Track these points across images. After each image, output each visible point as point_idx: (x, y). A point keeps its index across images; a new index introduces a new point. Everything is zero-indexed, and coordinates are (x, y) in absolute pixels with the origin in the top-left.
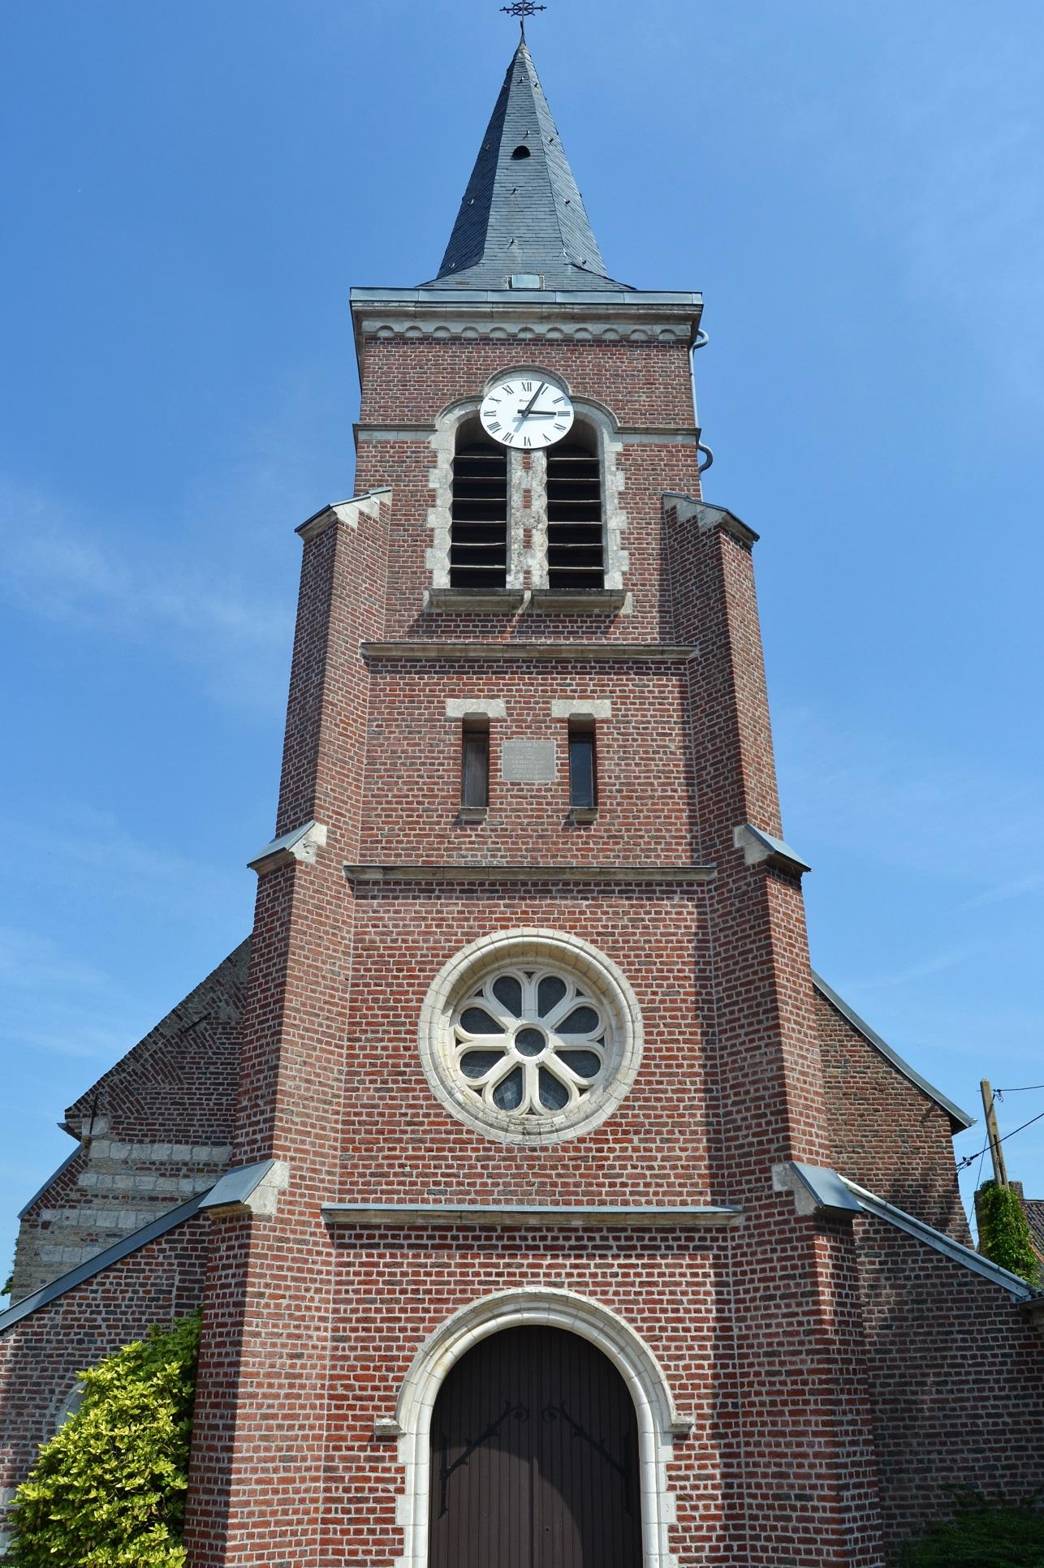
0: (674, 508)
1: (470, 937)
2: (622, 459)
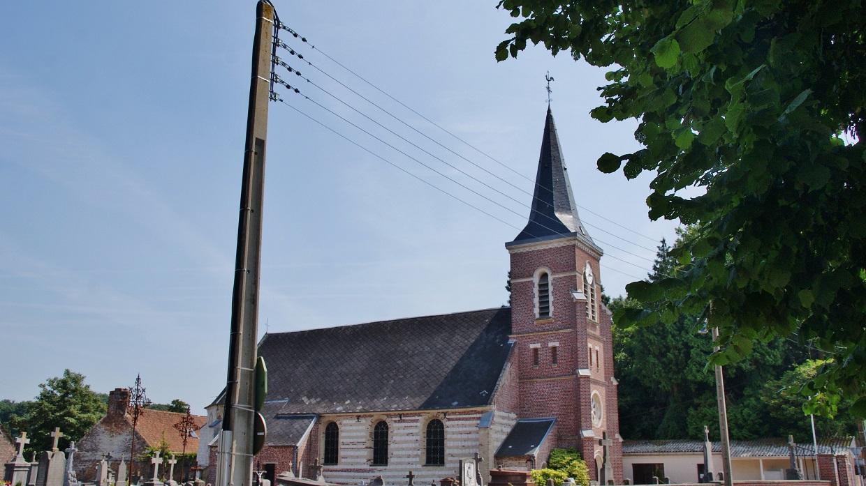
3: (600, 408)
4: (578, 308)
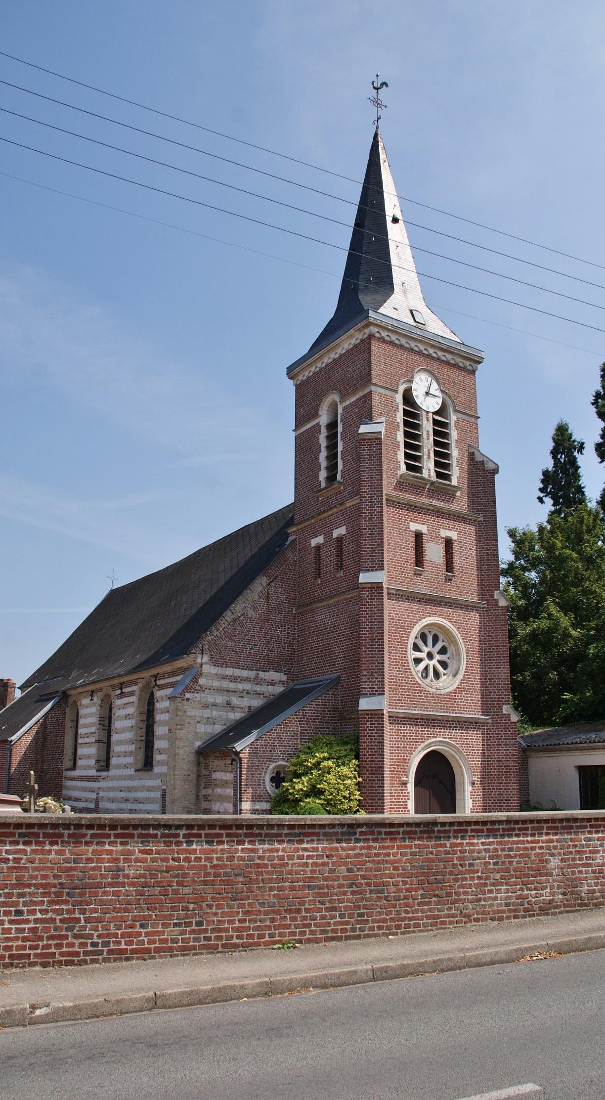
1: (421, 619)
2: (457, 422)
3: (459, 654)
4: (365, 450)
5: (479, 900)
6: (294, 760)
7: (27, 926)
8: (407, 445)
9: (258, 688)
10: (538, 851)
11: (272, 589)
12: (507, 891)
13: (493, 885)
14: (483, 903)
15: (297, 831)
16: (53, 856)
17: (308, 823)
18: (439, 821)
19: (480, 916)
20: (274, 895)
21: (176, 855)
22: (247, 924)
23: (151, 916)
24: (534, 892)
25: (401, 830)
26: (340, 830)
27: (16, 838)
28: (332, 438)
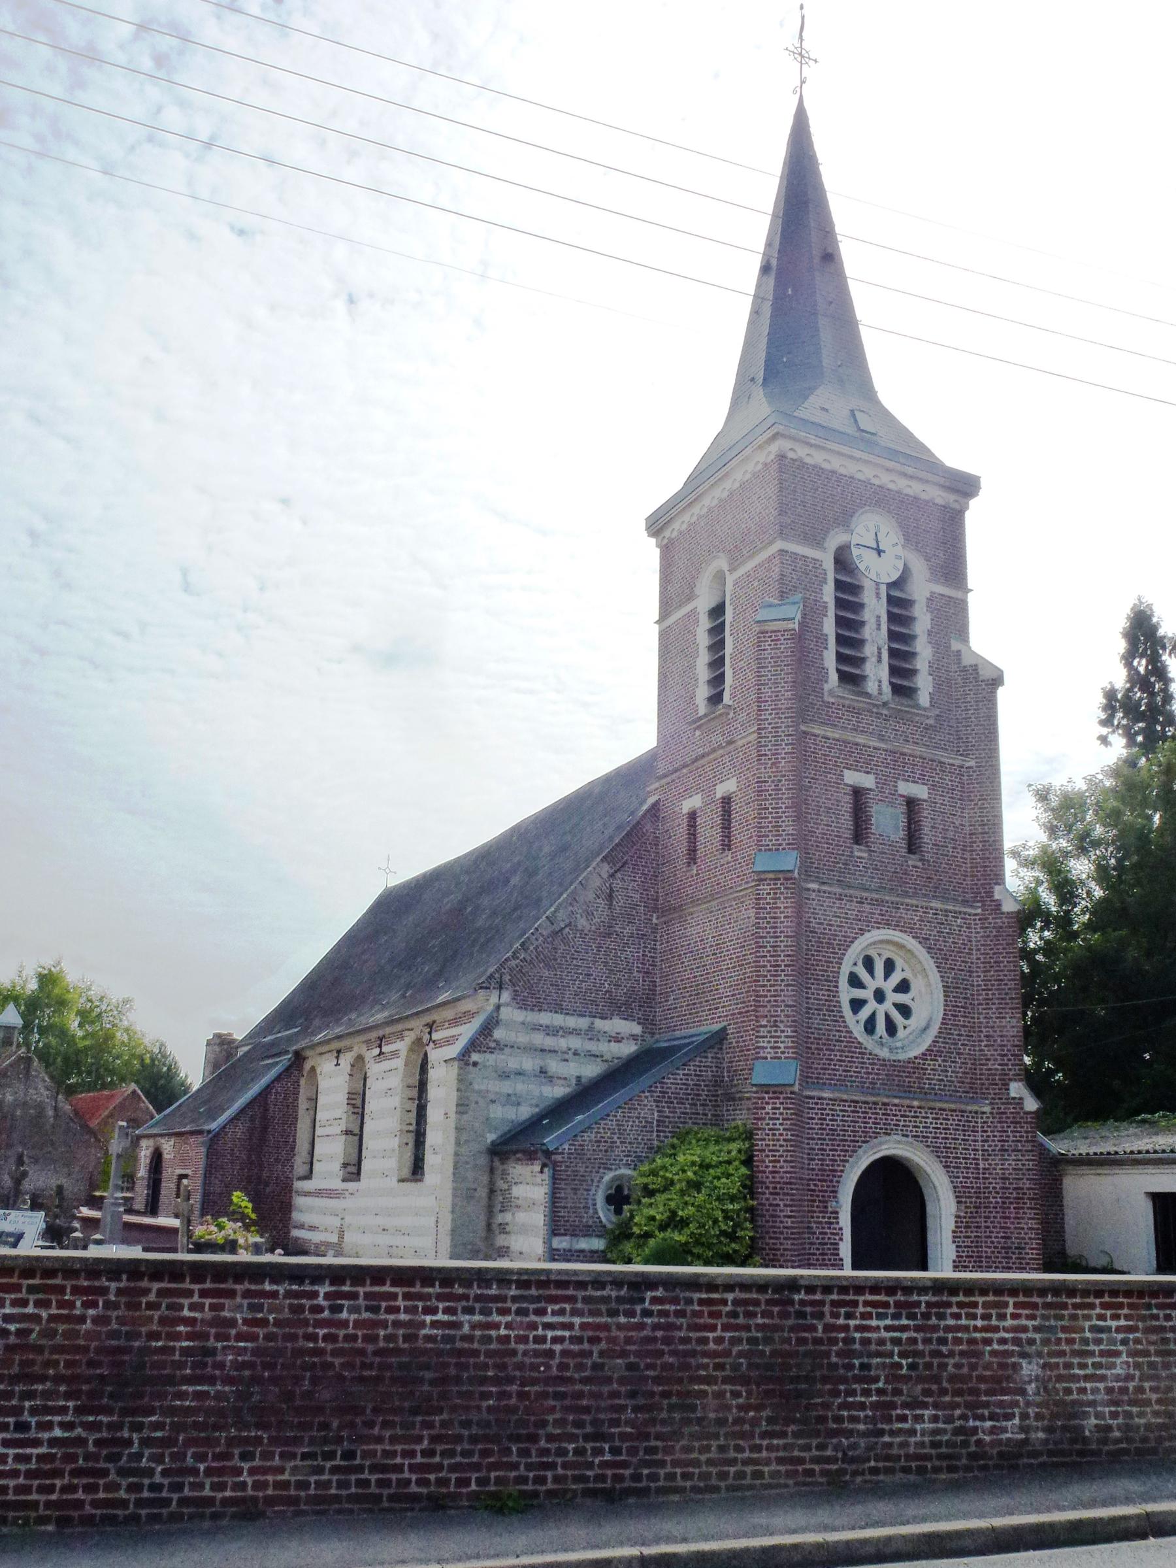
0: (959, 651)
5: (881, 1433)
6: (645, 1168)
7: (35, 1451)
8: (841, 640)
9: (592, 1046)
10: (996, 1346)
11: (617, 884)
12: (935, 1419)
13: (905, 1405)
14: (887, 1439)
15: (533, 1292)
16: (89, 1325)
17: (553, 1277)
18: (802, 1282)
19: (881, 1465)
20: (489, 1408)
21: (310, 1330)
22: (437, 1459)
23: (261, 1438)
24: (989, 1424)
25: (730, 1297)
26: (614, 1294)
27: (23, 1294)
28: (718, 630)
